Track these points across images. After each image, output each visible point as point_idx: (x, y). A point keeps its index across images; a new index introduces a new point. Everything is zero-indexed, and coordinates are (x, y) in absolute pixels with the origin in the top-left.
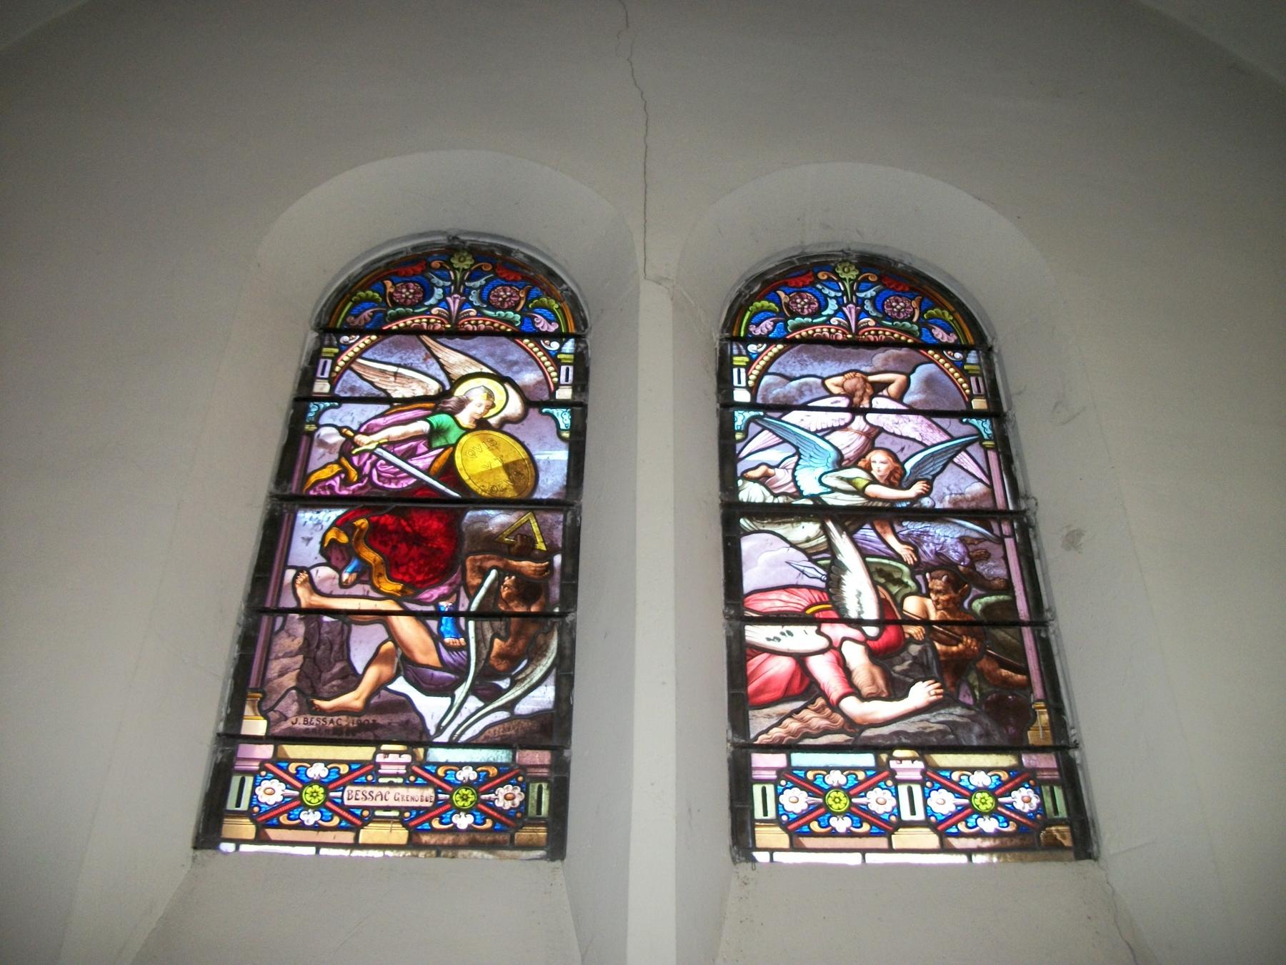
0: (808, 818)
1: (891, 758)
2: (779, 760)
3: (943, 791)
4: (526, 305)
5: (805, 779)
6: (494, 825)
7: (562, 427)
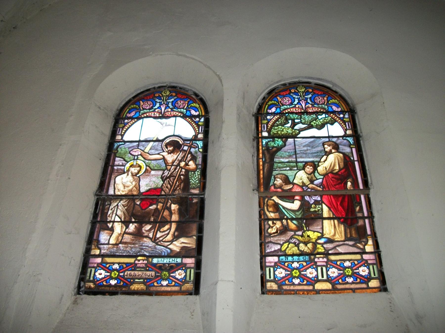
2: (276, 259)
3: (334, 268)
4: (188, 106)
5: (105, 267)
6: (360, 280)
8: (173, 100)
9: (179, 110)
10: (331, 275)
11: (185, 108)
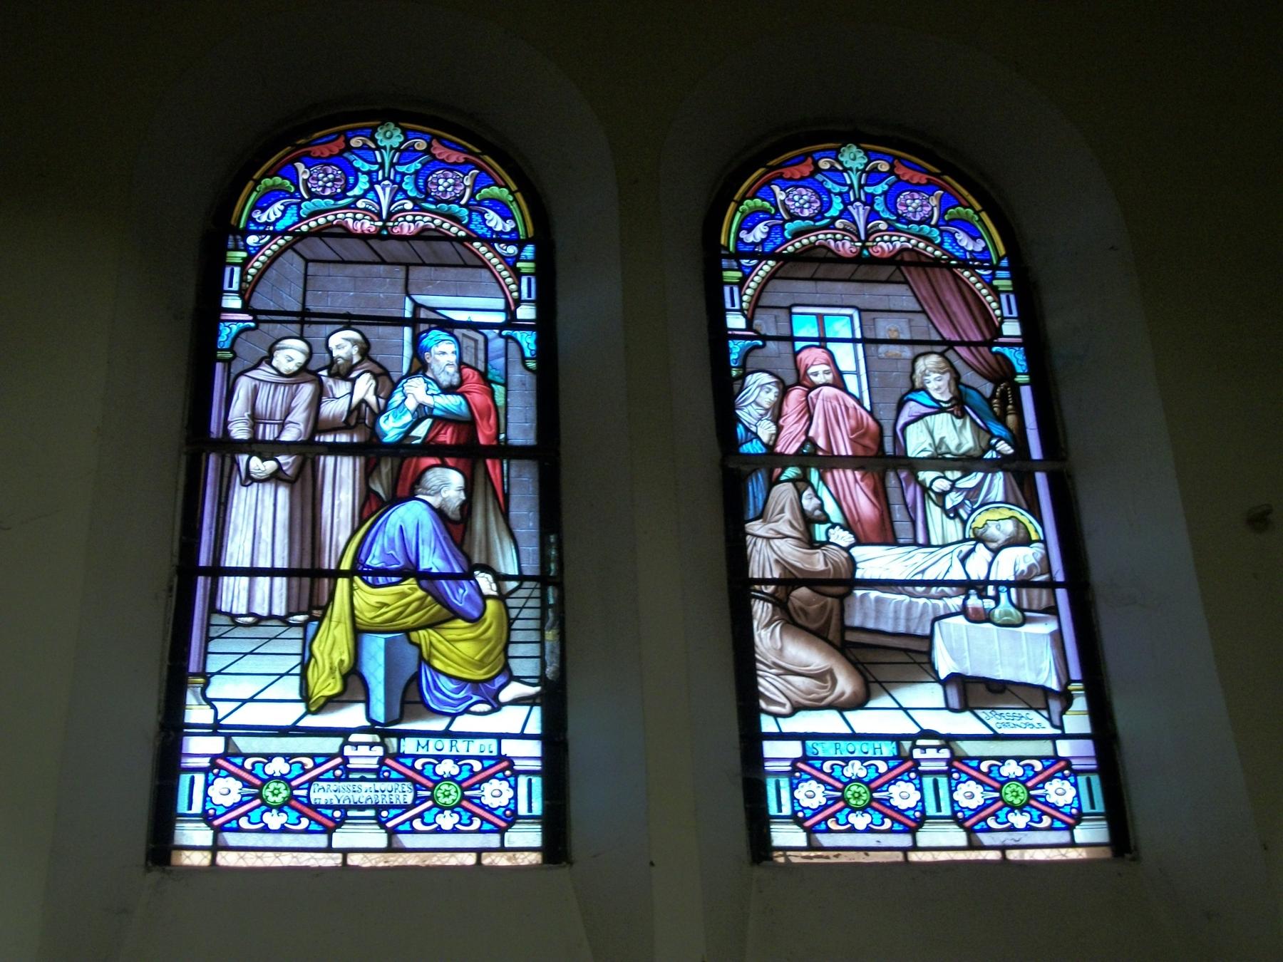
0: (983, 814)
1: (914, 746)
4: (472, 196)
7: (528, 354)
8: (417, 165)
9: (444, 206)
10: (964, 803)
11: (463, 202)
